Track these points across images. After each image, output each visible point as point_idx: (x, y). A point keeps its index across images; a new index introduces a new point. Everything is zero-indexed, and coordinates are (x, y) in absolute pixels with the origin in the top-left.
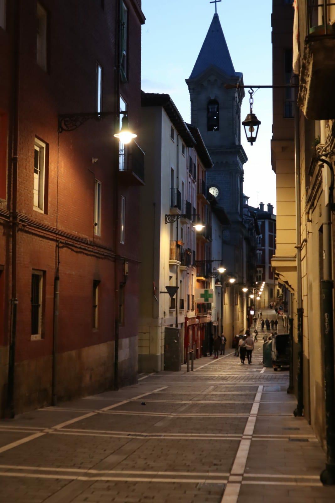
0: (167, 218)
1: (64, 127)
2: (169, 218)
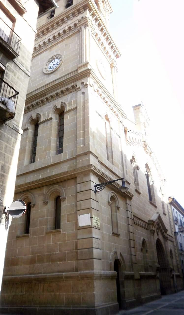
2: (98, 187)
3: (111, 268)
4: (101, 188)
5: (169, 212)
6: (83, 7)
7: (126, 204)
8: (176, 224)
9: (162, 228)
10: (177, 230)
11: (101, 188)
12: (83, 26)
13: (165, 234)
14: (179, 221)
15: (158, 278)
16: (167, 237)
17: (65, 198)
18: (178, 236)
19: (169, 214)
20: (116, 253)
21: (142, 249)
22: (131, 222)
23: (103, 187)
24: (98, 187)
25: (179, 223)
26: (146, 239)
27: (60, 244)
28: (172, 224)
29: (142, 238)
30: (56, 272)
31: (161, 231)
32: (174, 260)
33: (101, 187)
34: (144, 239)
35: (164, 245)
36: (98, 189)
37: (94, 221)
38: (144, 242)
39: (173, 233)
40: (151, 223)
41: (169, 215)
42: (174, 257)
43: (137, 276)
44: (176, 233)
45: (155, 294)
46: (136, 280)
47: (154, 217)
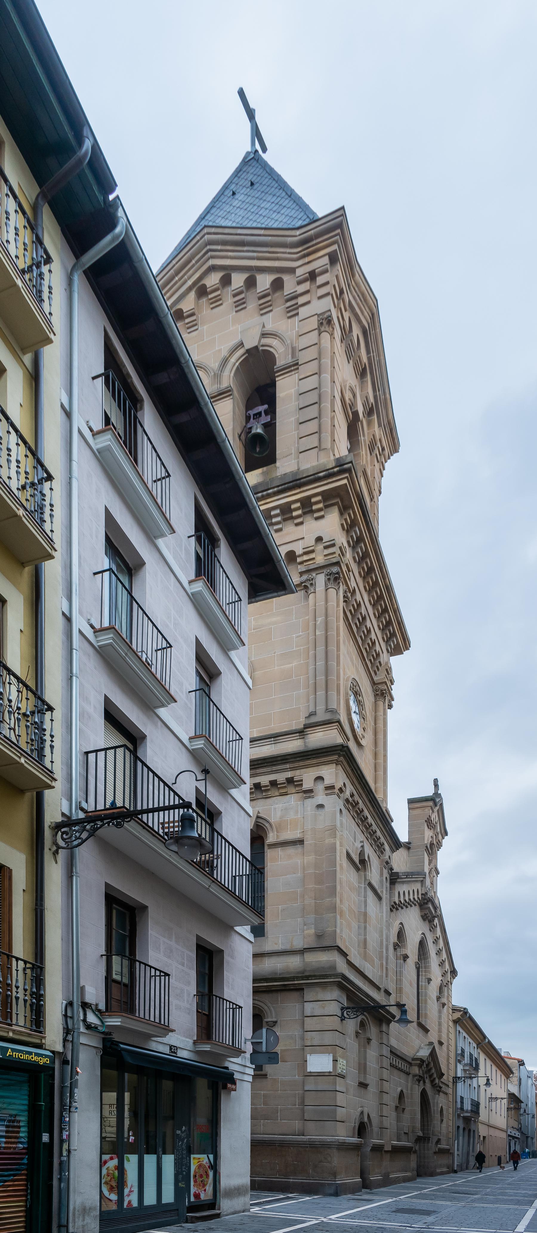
0: (60, 833)
1: (347, 1017)
2: (63, 833)
3: (354, 1133)
4: (79, 838)
5: (449, 1038)
6: (321, 494)
7: (381, 1031)
8: (460, 1061)
9: (433, 1071)
10: (459, 1074)
11: (77, 838)
12: (319, 576)
13: (437, 1081)
14: (467, 1055)
15: (415, 1152)
16: (441, 1087)
17: (276, 1022)
18: (460, 1085)
19: (448, 1041)
20: (362, 1113)
21: (397, 1107)
22: (386, 1063)
23: (84, 835)
24: (63, 830)
25: (467, 1060)
26: (404, 1091)
27: (264, 1094)
28: (452, 1061)
29: (399, 1089)
30: (261, 1134)
31: (431, 1076)
32: (444, 1125)
33: (78, 834)
34: (402, 1091)
35: (431, 1101)
36: (63, 839)
37: (339, 1066)
38: (401, 1095)
39: (451, 1080)
40: (421, 1062)
41: (449, 1045)
42: (445, 1120)
43: (388, 1148)
44: (456, 1079)
45: (409, 1174)
46: (387, 1152)
47: (424, 1053)
